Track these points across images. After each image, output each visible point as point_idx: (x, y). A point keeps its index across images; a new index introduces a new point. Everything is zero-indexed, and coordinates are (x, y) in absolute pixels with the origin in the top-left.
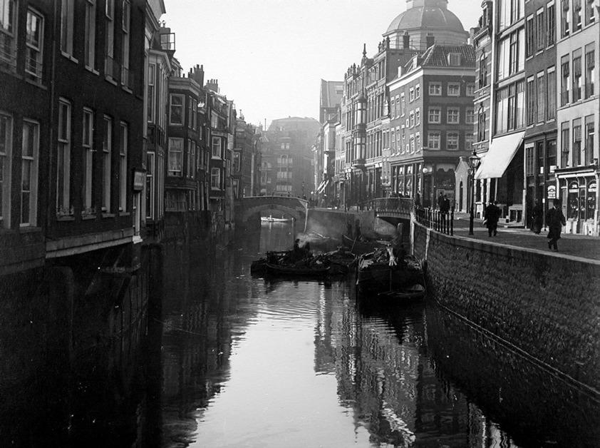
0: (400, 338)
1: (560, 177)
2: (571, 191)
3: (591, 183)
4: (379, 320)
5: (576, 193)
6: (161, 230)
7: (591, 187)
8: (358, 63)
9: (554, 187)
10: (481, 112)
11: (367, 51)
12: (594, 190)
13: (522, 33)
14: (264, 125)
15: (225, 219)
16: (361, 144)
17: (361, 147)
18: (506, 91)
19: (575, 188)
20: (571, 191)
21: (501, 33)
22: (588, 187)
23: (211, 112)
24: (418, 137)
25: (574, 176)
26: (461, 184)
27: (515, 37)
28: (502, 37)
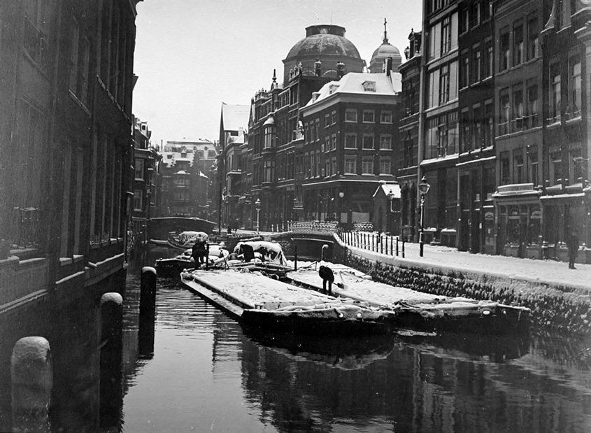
0: (102, 340)
1: (500, 204)
2: (510, 218)
3: (534, 210)
4: (376, 313)
5: (518, 220)
6: (119, 222)
7: (533, 214)
8: (268, 89)
9: (492, 214)
10: (408, 139)
11: (277, 76)
12: (537, 217)
13: (454, 67)
14: (160, 146)
15: (448, 168)
16: (271, 167)
17: (271, 170)
18: (436, 121)
19: (515, 215)
20: (510, 218)
21: (429, 65)
22: (531, 215)
23: (453, 12)
24: (334, 162)
25: (516, 203)
26: (381, 209)
27: (445, 70)
28: (429, 69)
